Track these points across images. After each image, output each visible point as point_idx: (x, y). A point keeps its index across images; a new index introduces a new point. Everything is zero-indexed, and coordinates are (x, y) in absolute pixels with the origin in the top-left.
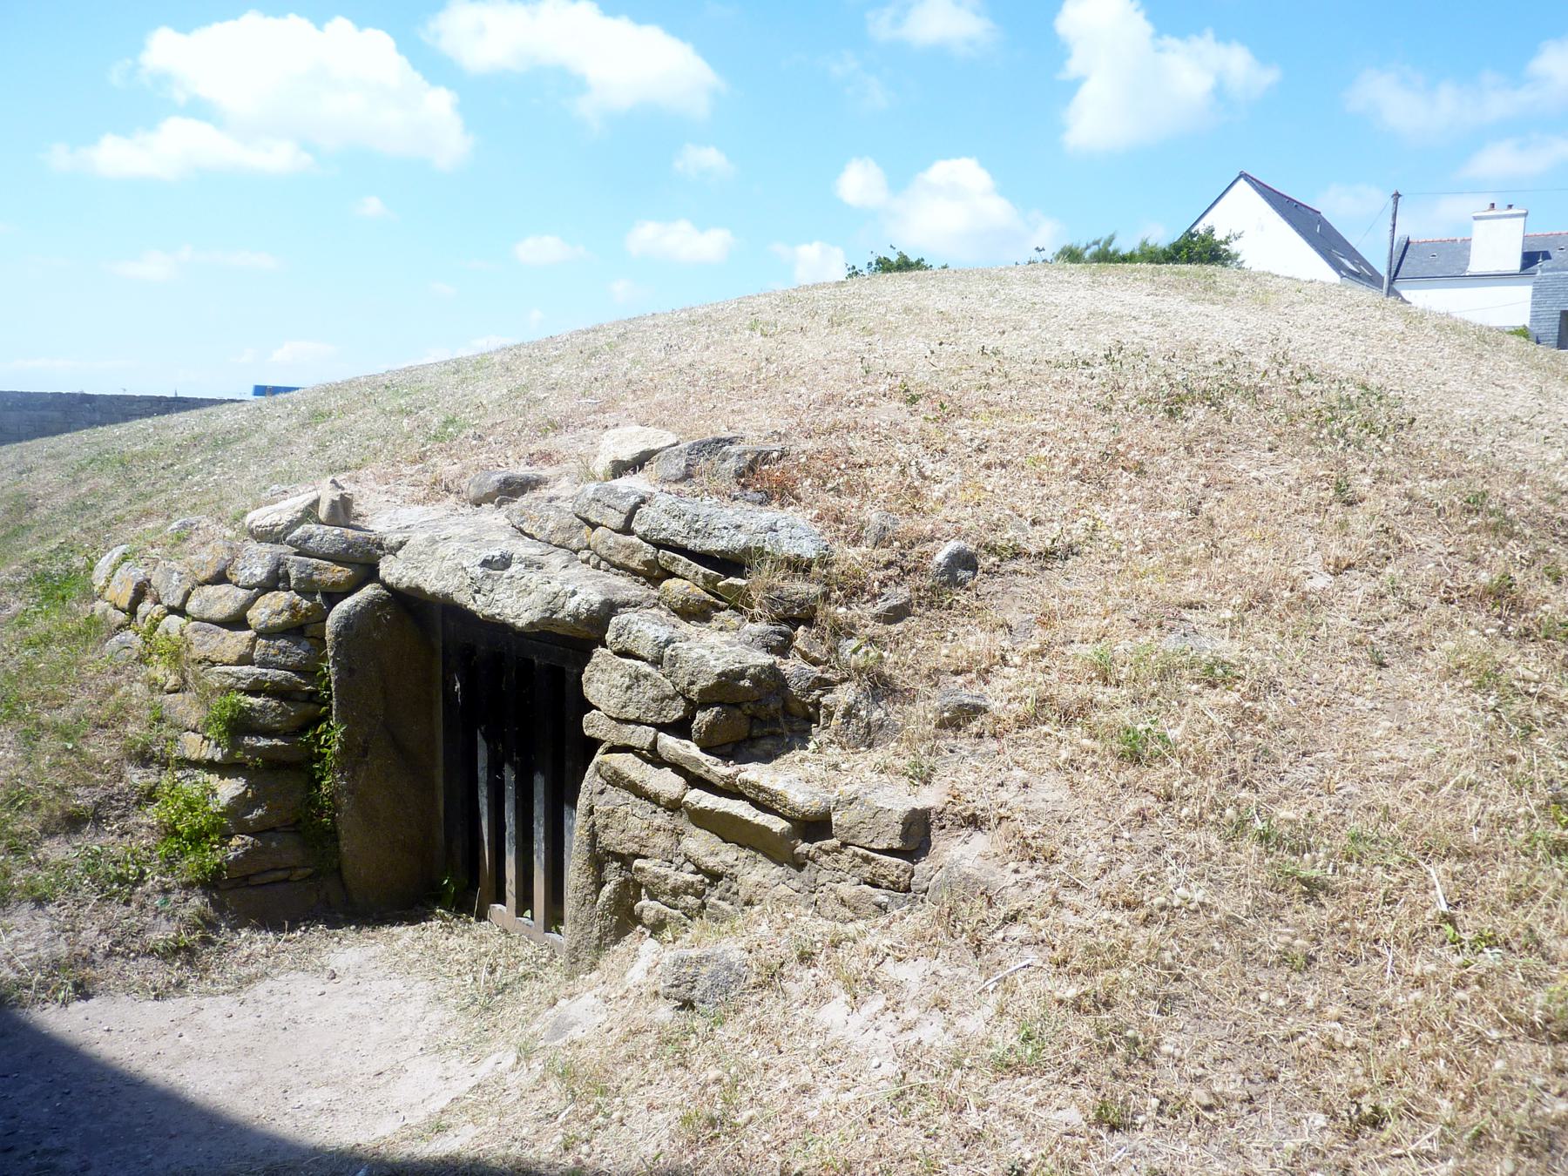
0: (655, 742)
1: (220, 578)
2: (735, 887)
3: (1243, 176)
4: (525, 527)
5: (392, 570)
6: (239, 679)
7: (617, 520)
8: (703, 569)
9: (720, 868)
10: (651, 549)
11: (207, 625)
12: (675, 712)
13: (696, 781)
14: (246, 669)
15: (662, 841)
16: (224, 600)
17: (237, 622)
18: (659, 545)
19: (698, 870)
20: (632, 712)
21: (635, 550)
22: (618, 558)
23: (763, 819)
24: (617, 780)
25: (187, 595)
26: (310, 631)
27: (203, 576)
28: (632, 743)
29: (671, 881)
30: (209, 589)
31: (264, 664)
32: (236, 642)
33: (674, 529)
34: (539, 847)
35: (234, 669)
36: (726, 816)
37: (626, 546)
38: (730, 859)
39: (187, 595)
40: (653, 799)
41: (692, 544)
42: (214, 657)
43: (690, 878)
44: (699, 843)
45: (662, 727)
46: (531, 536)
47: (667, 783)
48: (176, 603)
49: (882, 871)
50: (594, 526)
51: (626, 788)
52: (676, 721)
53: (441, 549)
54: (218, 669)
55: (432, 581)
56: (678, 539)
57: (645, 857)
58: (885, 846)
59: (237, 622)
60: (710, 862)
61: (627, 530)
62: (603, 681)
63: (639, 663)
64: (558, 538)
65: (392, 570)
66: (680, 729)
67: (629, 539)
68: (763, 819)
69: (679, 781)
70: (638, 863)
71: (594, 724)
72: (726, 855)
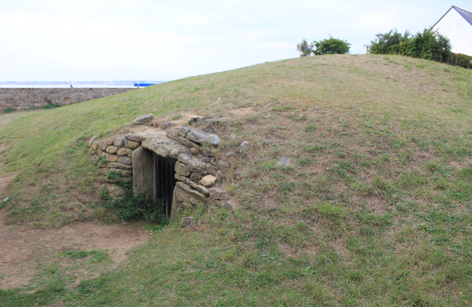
1: (112, 144)
3: (453, 7)
5: (144, 144)
7: (184, 135)
12: (188, 174)
13: (192, 188)
14: (116, 163)
15: (186, 199)
16: (112, 149)
17: (115, 154)
18: (191, 140)
19: (192, 204)
20: (182, 174)
21: (186, 141)
22: (184, 143)
23: (200, 194)
24: (180, 187)
25: (106, 148)
26: (129, 155)
27: (109, 144)
30: (110, 147)
31: (120, 163)
32: (114, 158)
33: (192, 137)
39: (106, 148)
40: (184, 190)
41: (195, 141)
43: (190, 205)
44: (192, 199)
47: (187, 188)
48: (104, 149)
53: (157, 139)
54: (111, 163)
55: (151, 147)
59: (115, 154)
60: (193, 202)
61: (185, 137)
62: (178, 168)
64: (174, 138)
65: (144, 144)
66: (188, 177)
67: (186, 139)
68: (200, 194)
69: (114, 169)
70: (183, 203)
71: (176, 176)
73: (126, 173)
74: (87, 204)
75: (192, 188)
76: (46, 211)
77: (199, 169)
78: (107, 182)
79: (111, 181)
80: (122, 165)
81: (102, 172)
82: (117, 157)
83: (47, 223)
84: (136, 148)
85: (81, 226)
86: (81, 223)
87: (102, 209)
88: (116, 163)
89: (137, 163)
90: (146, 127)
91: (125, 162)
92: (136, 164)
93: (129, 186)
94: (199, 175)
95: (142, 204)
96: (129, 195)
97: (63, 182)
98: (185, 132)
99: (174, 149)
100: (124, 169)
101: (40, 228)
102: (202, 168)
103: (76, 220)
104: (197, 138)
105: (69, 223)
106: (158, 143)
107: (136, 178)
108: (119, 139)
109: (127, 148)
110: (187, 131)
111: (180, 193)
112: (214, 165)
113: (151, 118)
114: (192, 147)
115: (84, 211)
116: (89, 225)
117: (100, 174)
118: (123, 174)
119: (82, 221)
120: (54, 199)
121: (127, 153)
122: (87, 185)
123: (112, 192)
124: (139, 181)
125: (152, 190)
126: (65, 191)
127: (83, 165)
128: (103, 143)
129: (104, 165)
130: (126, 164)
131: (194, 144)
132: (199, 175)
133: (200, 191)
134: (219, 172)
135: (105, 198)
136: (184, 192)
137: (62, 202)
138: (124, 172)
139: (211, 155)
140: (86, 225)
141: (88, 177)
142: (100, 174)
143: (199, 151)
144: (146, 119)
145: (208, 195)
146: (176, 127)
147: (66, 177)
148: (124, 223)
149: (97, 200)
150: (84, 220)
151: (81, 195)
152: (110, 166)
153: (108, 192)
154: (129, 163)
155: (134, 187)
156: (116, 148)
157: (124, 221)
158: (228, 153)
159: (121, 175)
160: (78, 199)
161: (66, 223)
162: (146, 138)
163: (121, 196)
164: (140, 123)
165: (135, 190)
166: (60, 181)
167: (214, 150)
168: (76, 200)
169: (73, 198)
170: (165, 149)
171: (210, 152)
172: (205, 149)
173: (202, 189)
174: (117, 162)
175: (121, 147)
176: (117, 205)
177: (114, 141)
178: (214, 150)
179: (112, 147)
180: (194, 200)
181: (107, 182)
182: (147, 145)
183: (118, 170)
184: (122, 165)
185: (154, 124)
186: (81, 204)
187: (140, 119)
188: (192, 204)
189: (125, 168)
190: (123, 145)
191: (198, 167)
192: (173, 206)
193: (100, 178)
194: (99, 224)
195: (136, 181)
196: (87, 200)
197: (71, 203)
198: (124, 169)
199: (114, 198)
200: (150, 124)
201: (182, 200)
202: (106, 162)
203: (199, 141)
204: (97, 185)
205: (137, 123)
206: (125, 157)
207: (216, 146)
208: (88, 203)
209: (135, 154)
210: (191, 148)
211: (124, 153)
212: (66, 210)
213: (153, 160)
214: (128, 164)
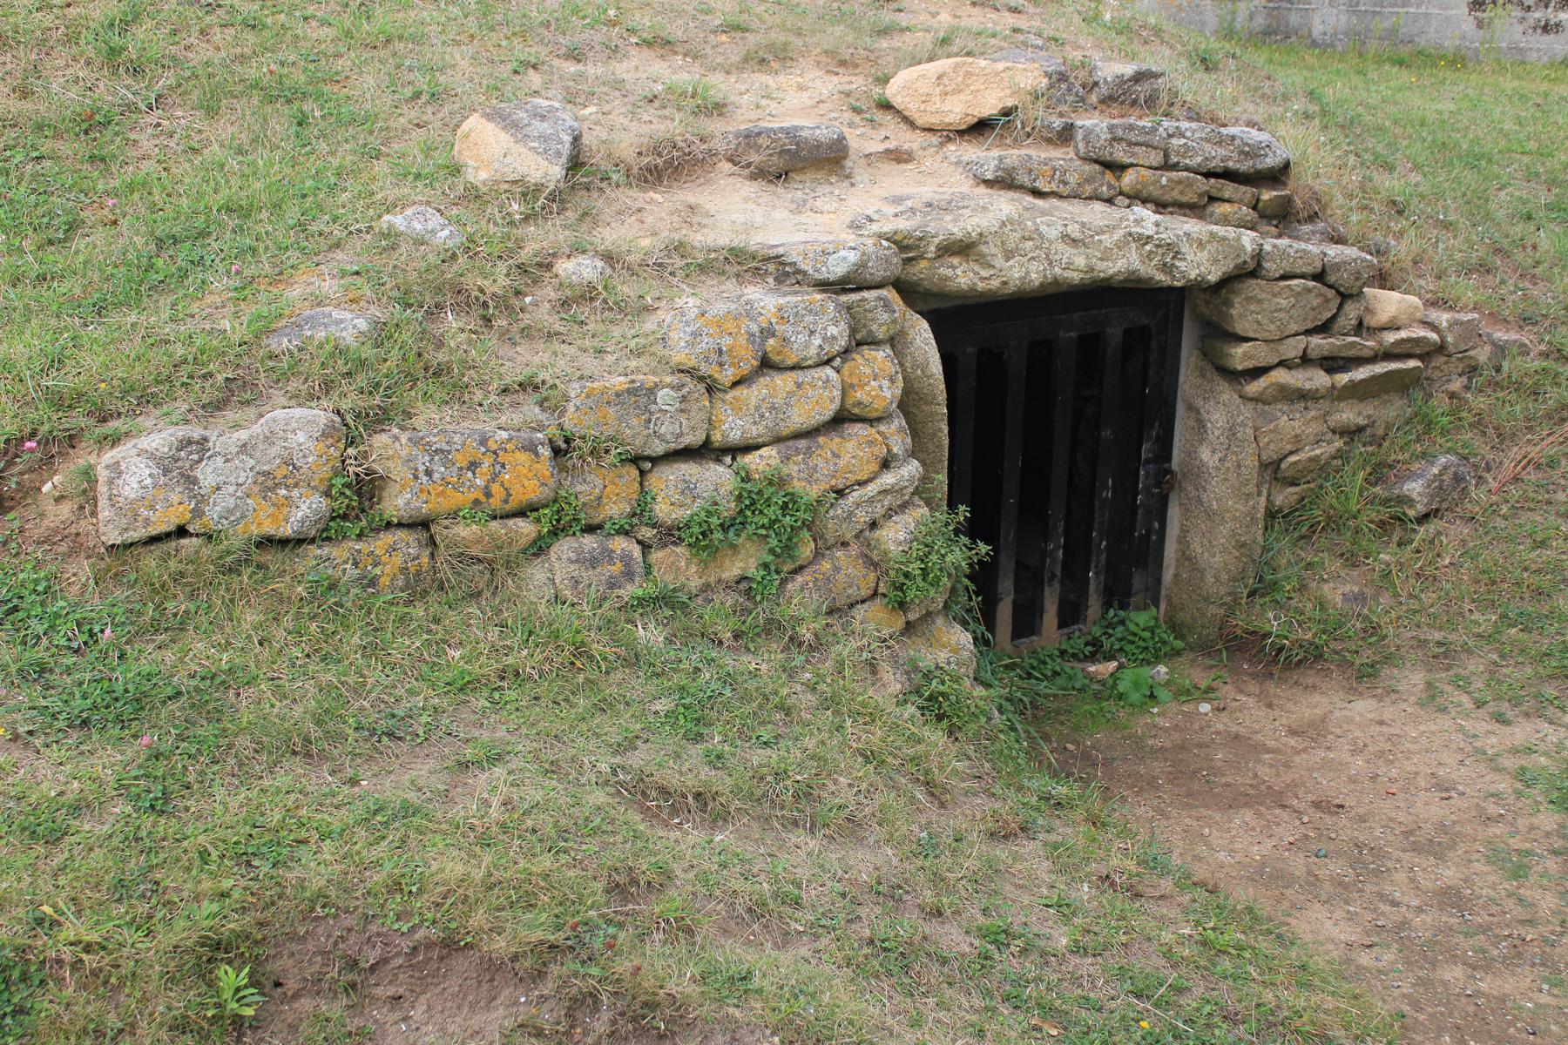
18: (1208, 175)
21: (1189, 184)
30: (753, 394)
36: (1375, 379)
37: (1180, 182)
46: (1053, 194)
47: (1318, 379)
64: (1088, 190)
104: (1252, 152)
131: (1229, 189)
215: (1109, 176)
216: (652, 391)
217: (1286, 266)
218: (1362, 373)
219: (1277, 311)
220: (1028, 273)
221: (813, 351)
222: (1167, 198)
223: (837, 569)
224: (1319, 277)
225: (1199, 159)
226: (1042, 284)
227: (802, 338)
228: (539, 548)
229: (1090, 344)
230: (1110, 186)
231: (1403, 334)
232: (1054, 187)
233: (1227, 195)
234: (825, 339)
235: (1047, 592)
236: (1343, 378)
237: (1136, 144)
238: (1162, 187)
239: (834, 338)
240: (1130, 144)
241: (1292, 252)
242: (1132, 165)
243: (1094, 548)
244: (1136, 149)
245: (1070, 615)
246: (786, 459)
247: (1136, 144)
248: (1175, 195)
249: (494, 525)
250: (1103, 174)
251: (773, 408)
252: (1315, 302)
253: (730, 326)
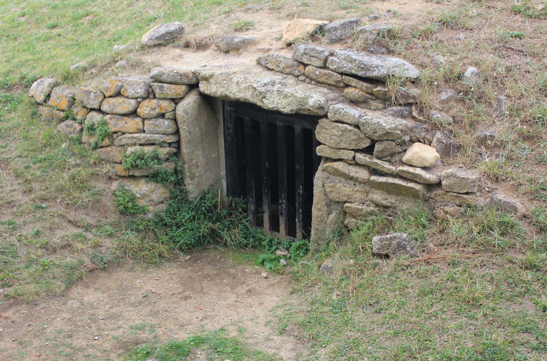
0: (354, 158)
2: (395, 211)
4: (268, 65)
5: (203, 87)
6: (139, 139)
7: (320, 63)
8: (366, 84)
9: (389, 204)
10: (339, 76)
11: (117, 116)
12: (366, 144)
13: (375, 172)
14: (143, 135)
15: (358, 195)
16: (128, 105)
17: (134, 113)
18: (342, 74)
20: (343, 145)
21: (330, 76)
24: (337, 173)
27: (107, 94)
28: (343, 157)
29: (364, 211)
30: (112, 100)
31: (151, 133)
32: (132, 124)
33: (348, 67)
34: (299, 201)
35: (136, 135)
36: (386, 184)
37: (325, 74)
38: (393, 201)
39: (101, 103)
41: (360, 74)
42: (123, 131)
44: (378, 196)
45: (356, 151)
46: (272, 70)
47: (363, 174)
48: (96, 106)
49: (464, 201)
50: (306, 65)
51: (340, 175)
52: (367, 147)
54: (127, 135)
56: (353, 72)
57: (350, 202)
58: (465, 191)
59: (134, 113)
60: (384, 203)
61: (324, 67)
62: (326, 135)
63: (345, 125)
64: (288, 70)
67: (326, 71)
69: (138, 148)
71: (320, 151)
72: (391, 200)
73: (168, 153)
74: (94, 230)
75: (375, 172)
76: (12, 260)
77: (399, 132)
78: (123, 177)
79: (137, 173)
80: (156, 136)
81: (103, 157)
82: (138, 120)
83: (32, 288)
84: (182, 98)
85: (104, 280)
86: (102, 274)
87: (133, 237)
88: (139, 137)
89: (192, 130)
90: (178, 51)
91: (162, 129)
92: (190, 132)
93: (177, 180)
94: (392, 146)
95: (210, 212)
96: (178, 196)
97: (17, 187)
98: (322, 56)
99: (315, 97)
100: (162, 145)
101: (22, 302)
102: (402, 131)
103: (91, 271)
104: (366, 68)
105: (81, 278)
106: (265, 84)
107: (191, 160)
108: (136, 82)
109: (160, 99)
110: (326, 53)
111: (339, 185)
112: (420, 121)
113: (181, 31)
114: (347, 86)
115: (97, 246)
116: (121, 275)
117: (99, 162)
118: (162, 156)
119: (104, 269)
120: (14, 229)
121: (163, 111)
122: (82, 189)
123: (143, 196)
124: (197, 167)
125: (218, 181)
126: (32, 208)
127: (45, 146)
128: (89, 92)
129: (107, 141)
130: (164, 134)
131: (354, 82)
132: (392, 146)
133: (413, 178)
134: (439, 135)
135: (129, 210)
136: (352, 183)
137: (38, 234)
138: (163, 152)
139: (411, 101)
140: (115, 276)
141: (74, 171)
142: (99, 162)
143: (371, 94)
144: (171, 33)
145: (430, 186)
146: (260, 47)
147: (18, 176)
148: (184, 257)
149: (114, 218)
150: (104, 267)
151: (72, 213)
152: (124, 141)
153: (133, 199)
154: (171, 130)
155: (187, 181)
156: (133, 102)
157: (182, 254)
158: (444, 93)
159: (156, 157)
160: (70, 221)
161: (74, 279)
162: (211, 76)
163: (162, 202)
164: (158, 42)
165: (192, 188)
166: (9, 188)
167: (414, 91)
168: (65, 224)
169: (57, 220)
170: (286, 96)
171: (408, 96)
172: (391, 89)
173: (418, 175)
174: (144, 131)
175: (144, 99)
176: (161, 223)
177: (122, 87)
178: (414, 91)
179: (120, 99)
180: (385, 195)
181: (123, 177)
182: (222, 89)
183: (148, 150)
184: (156, 136)
185: (193, 42)
186: (80, 231)
187: (157, 35)
188: (377, 205)
189: (165, 142)
190: (150, 94)
191: (396, 128)
192: (315, 212)
193: (105, 171)
194: (138, 268)
195: (190, 166)
196: (93, 222)
197: (58, 232)
198: (162, 145)
199: (151, 208)
200: (182, 42)
201: (345, 199)
202: (110, 136)
203: (375, 74)
204: (100, 185)
205: (151, 43)
206: (161, 120)
207: (414, 82)
208: (96, 226)
209: (185, 112)
210: (347, 90)
211: (158, 110)
212: (55, 251)
213: (218, 120)
214: (168, 134)
215: (301, 67)
216: (90, 92)
217: (338, 117)
218: (390, 180)
219: (333, 135)
220: (217, 91)
221: (131, 94)
222: (320, 80)
223: (112, 151)
224: (357, 126)
225: (335, 67)
226: (221, 95)
227: (131, 90)
228: (62, 120)
229: (290, 130)
230: (299, 71)
231: (411, 170)
232: (273, 67)
233: (353, 84)
234: (135, 92)
235: (280, 218)
236: (373, 178)
237: (313, 57)
238: (317, 75)
239: (138, 93)
240: (310, 56)
241: (343, 112)
242: (310, 65)
243: (297, 211)
244: (312, 59)
245: (291, 232)
246: (111, 119)
247: (313, 57)
248: (323, 79)
249: (58, 111)
250: (299, 66)
251: (114, 105)
252: (354, 137)
253: (114, 82)
